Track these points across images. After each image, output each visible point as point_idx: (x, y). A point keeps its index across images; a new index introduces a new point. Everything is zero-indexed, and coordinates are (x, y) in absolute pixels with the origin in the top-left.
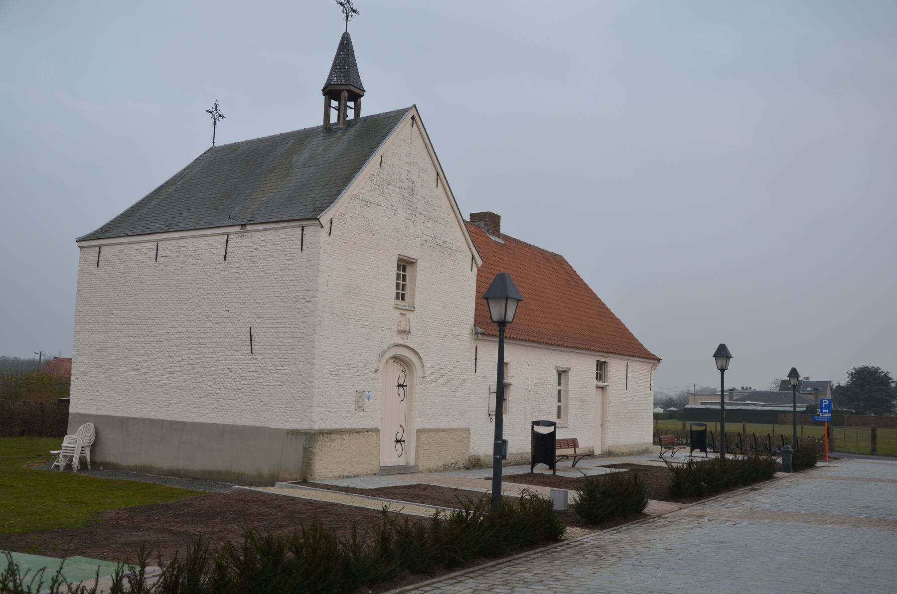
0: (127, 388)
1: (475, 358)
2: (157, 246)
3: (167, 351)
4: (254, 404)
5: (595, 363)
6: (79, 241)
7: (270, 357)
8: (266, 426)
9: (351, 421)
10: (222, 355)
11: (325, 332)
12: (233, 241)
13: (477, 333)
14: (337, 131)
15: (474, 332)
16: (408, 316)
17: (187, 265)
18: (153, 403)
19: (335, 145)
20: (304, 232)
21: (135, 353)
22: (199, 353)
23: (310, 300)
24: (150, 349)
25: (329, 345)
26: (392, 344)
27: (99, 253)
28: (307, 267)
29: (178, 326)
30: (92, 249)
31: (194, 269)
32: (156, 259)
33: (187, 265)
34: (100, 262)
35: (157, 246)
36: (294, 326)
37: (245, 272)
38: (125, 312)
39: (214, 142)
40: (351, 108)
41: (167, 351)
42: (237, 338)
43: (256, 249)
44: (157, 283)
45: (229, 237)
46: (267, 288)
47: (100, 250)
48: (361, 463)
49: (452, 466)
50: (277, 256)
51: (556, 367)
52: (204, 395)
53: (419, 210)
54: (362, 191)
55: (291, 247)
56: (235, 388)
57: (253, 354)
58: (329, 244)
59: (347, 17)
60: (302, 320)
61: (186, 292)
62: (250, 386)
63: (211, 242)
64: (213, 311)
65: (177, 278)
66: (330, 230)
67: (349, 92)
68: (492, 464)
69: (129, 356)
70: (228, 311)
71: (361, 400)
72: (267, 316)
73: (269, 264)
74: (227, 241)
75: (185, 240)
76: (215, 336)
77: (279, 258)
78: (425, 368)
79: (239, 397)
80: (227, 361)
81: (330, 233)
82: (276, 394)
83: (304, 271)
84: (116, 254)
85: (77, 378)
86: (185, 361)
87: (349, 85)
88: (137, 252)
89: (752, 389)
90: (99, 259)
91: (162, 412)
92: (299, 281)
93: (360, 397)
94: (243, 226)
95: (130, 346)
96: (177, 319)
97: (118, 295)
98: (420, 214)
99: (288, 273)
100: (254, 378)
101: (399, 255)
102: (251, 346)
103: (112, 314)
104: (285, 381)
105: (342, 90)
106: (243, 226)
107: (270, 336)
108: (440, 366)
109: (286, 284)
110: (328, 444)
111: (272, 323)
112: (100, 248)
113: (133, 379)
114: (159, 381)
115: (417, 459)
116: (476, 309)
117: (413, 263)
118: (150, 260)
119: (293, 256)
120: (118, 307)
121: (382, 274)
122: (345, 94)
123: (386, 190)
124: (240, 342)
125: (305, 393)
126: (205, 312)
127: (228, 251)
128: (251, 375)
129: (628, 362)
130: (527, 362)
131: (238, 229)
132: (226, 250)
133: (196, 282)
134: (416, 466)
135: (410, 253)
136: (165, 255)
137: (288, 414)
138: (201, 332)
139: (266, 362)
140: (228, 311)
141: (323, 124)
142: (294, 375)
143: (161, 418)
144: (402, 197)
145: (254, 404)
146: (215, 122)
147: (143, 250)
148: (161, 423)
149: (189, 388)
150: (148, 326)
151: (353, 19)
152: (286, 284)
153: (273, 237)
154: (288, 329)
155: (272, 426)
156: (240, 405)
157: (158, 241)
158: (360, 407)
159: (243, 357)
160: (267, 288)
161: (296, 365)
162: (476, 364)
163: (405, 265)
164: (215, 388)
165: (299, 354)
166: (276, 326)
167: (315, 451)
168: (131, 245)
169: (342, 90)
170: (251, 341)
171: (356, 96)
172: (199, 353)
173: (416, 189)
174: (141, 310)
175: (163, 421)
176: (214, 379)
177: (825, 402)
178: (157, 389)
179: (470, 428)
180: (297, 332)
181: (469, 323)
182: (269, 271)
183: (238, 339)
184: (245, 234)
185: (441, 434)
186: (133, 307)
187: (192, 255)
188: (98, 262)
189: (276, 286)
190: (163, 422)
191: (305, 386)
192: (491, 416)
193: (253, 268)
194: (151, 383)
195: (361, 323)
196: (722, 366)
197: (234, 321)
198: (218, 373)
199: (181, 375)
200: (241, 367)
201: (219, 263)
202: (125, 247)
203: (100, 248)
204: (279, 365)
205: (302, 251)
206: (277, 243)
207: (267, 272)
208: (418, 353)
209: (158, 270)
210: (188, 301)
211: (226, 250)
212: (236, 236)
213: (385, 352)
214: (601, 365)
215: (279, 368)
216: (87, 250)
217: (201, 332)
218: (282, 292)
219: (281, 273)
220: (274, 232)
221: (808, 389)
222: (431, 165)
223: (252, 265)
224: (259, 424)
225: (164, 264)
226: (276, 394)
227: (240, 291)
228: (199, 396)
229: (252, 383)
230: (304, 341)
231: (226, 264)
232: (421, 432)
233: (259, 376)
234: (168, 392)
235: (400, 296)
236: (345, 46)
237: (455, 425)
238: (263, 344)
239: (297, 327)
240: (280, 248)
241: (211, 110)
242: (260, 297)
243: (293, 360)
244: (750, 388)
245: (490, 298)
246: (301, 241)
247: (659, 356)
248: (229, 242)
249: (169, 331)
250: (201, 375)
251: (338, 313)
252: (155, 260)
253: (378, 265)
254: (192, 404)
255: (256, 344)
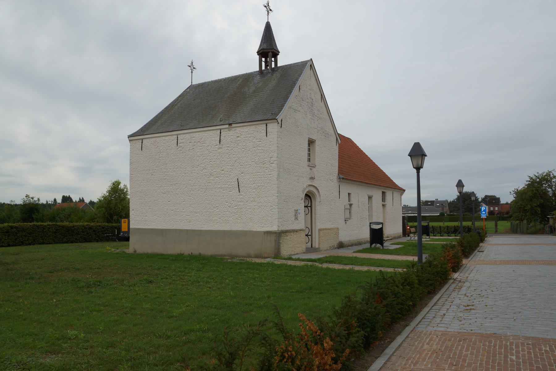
0: (164, 214)
1: (339, 191)
2: (177, 137)
3: (187, 193)
4: (243, 219)
5: (381, 193)
6: (129, 136)
7: (250, 194)
8: (250, 230)
9: (293, 226)
10: (221, 194)
11: (281, 179)
12: (223, 133)
13: (340, 178)
14: (267, 74)
15: (338, 178)
16: (313, 170)
17: (196, 147)
18: (181, 221)
19: (269, 81)
20: (267, 127)
21: (167, 195)
22: (207, 193)
23: (273, 162)
24: (177, 193)
25: (283, 186)
26: (307, 185)
27: (142, 142)
28: (270, 145)
29: (193, 180)
30: (137, 141)
31: (201, 149)
32: (177, 144)
33: (196, 147)
34: (143, 147)
35: (177, 137)
36: (264, 176)
37: (233, 149)
38: (160, 173)
39: (192, 82)
40: (273, 61)
41: (187, 193)
42: (230, 184)
43: (238, 137)
44: (179, 157)
45: (221, 131)
46: (247, 157)
47: (142, 141)
48: (299, 247)
49: (333, 247)
50: (252, 140)
51: (368, 195)
52: (211, 215)
53: (315, 114)
54: (293, 104)
55: (259, 135)
56: (230, 211)
57: (240, 193)
58: (281, 132)
59: (268, 13)
60: (269, 173)
61: (197, 161)
62: (239, 209)
63: (211, 134)
64: (214, 171)
65: (191, 154)
66: (281, 125)
67: (273, 52)
68: (417, 240)
69: (164, 197)
70: (223, 170)
71: (296, 215)
72: (247, 172)
73: (246, 144)
74: (220, 133)
75: (195, 133)
76: (216, 184)
77: (253, 141)
78: (321, 197)
79: (233, 216)
80: (224, 197)
81: (281, 127)
82: (256, 213)
83: (269, 147)
84: (152, 143)
85: (133, 210)
86: (199, 198)
87: (272, 49)
88: (165, 141)
89: (409, 206)
90: (142, 146)
91: (186, 225)
92: (266, 153)
93: (296, 213)
94: (230, 124)
95: (165, 191)
96: (192, 176)
97: (155, 165)
98: (316, 116)
99: (259, 149)
100: (241, 205)
101: (309, 138)
102: (239, 188)
103: (152, 175)
104: (260, 206)
105: (269, 52)
106: (230, 124)
107: (250, 183)
108: (326, 196)
109: (258, 155)
110: (285, 238)
111: (250, 176)
112: (142, 140)
113: (167, 209)
114: (183, 209)
115: (319, 244)
116: (339, 165)
117: (313, 142)
118: (174, 145)
119: (262, 139)
120: (155, 171)
121: (302, 148)
122: (270, 54)
123: (302, 103)
124: (231, 186)
125: (273, 212)
126: (209, 172)
127: (221, 138)
128: (240, 204)
129: (393, 192)
130: (357, 193)
131: (227, 126)
132: (220, 138)
133: (202, 156)
134: (319, 248)
135: (313, 137)
136: (183, 142)
137: (264, 223)
138: (207, 182)
139: (249, 196)
140: (223, 170)
141: (258, 70)
142: (266, 202)
143: (186, 229)
144: (308, 107)
145: (243, 219)
146: (192, 71)
147: (169, 140)
148: (187, 231)
149: (202, 212)
150: (175, 180)
151: (271, 13)
152: (258, 155)
153: (249, 130)
154: (261, 178)
155: (255, 230)
156: (234, 220)
157: (177, 135)
158: (296, 218)
159: (234, 194)
160: (247, 157)
161: (267, 197)
162: (339, 194)
163: (311, 142)
164: (218, 211)
165: (268, 191)
166: (254, 177)
167: (280, 241)
168: (161, 138)
169: (269, 52)
170: (238, 185)
171: (275, 54)
172: (207, 193)
173: (313, 103)
174: (170, 172)
175: (187, 230)
176: (217, 207)
177: (483, 208)
178: (182, 213)
179: (339, 227)
180: (266, 180)
181: (336, 173)
182: (247, 148)
183: (230, 185)
184: (231, 129)
185: (328, 231)
186: (164, 170)
187: (199, 141)
188: (142, 148)
189: (252, 156)
190: (187, 231)
191: (273, 208)
192: (346, 221)
193: (237, 147)
194: (178, 210)
195: (295, 174)
196: (460, 191)
197: (227, 175)
198: (219, 203)
199: (196, 205)
200: (233, 200)
201: (216, 145)
202: (158, 139)
203: (142, 140)
204: (256, 198)
205: (267, 137)
206: (251, 133)
207: (245, 148)
208: (318, 189)
209: (179, 150)
210: (198, 166)
211: (220, 138)
212: (226, 130)
213: (305, 189)
214: (384, 193)
215: (256, 199)
216: (134, 142)
217: (207, 182)
218: (255, 159)
219: (254, 149)
220: (249, 127)
221: (437, 205)
222: (319, 90)
223: (237, 145)
224: (246, 229)
225: (182, 147)
226: (256, 213)
227: (230, 159)
228: (209, 216)
229: (241, 208)
230: (271, 184)
231: (220, 145)
232: (320, 230)
233: (244, 204)
234: (189, 215)
235: (309, 160)
236: (268, 29)
237: (332, 226)
238: (245, 187)
239: (266, 177)
240: (253, 135)
241: (190, 65)
242: (242, 162)
243: (265, 195)
244: (408, 205)
245: (412, 155)
246: (266, 131)
247: (404, 188)
248: (221, 133)
249: (187, 182)
250: (209, 205)
251: (286, 169)
252: (176, 145)
253: (300, 143)
254: (205, 221)
255: (241, 187)
